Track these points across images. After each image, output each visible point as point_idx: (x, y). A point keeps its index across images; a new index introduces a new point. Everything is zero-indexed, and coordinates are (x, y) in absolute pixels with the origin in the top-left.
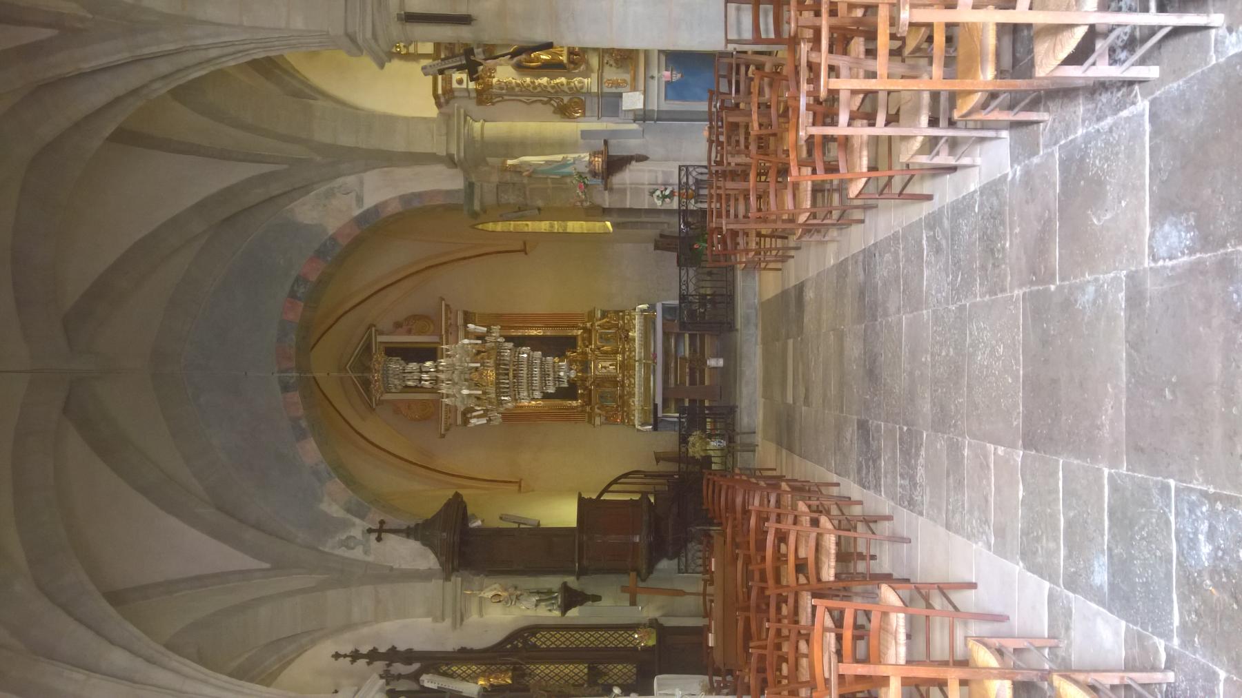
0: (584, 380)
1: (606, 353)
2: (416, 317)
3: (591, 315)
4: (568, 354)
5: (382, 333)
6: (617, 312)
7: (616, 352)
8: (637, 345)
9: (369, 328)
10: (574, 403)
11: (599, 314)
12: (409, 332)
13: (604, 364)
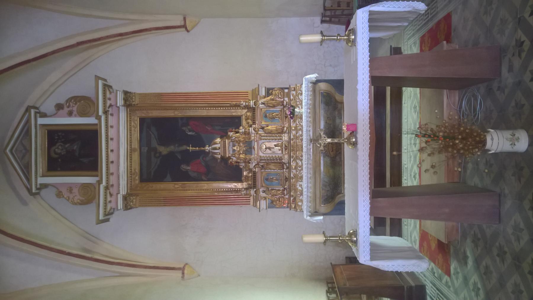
0: (247, 162)
1: (270, 132)
2: (76, 99)
3: (255, 93)
4: (231, 134)
5: (44, 115)
6: (283, 89)
7: (282, 132)
8: (304, 123)
9: (28, 109)
10: (239, 185)
11: (263, 92)
12: (70, 114)
13: (268, 145)
